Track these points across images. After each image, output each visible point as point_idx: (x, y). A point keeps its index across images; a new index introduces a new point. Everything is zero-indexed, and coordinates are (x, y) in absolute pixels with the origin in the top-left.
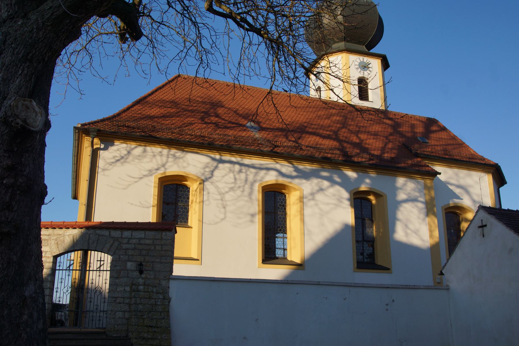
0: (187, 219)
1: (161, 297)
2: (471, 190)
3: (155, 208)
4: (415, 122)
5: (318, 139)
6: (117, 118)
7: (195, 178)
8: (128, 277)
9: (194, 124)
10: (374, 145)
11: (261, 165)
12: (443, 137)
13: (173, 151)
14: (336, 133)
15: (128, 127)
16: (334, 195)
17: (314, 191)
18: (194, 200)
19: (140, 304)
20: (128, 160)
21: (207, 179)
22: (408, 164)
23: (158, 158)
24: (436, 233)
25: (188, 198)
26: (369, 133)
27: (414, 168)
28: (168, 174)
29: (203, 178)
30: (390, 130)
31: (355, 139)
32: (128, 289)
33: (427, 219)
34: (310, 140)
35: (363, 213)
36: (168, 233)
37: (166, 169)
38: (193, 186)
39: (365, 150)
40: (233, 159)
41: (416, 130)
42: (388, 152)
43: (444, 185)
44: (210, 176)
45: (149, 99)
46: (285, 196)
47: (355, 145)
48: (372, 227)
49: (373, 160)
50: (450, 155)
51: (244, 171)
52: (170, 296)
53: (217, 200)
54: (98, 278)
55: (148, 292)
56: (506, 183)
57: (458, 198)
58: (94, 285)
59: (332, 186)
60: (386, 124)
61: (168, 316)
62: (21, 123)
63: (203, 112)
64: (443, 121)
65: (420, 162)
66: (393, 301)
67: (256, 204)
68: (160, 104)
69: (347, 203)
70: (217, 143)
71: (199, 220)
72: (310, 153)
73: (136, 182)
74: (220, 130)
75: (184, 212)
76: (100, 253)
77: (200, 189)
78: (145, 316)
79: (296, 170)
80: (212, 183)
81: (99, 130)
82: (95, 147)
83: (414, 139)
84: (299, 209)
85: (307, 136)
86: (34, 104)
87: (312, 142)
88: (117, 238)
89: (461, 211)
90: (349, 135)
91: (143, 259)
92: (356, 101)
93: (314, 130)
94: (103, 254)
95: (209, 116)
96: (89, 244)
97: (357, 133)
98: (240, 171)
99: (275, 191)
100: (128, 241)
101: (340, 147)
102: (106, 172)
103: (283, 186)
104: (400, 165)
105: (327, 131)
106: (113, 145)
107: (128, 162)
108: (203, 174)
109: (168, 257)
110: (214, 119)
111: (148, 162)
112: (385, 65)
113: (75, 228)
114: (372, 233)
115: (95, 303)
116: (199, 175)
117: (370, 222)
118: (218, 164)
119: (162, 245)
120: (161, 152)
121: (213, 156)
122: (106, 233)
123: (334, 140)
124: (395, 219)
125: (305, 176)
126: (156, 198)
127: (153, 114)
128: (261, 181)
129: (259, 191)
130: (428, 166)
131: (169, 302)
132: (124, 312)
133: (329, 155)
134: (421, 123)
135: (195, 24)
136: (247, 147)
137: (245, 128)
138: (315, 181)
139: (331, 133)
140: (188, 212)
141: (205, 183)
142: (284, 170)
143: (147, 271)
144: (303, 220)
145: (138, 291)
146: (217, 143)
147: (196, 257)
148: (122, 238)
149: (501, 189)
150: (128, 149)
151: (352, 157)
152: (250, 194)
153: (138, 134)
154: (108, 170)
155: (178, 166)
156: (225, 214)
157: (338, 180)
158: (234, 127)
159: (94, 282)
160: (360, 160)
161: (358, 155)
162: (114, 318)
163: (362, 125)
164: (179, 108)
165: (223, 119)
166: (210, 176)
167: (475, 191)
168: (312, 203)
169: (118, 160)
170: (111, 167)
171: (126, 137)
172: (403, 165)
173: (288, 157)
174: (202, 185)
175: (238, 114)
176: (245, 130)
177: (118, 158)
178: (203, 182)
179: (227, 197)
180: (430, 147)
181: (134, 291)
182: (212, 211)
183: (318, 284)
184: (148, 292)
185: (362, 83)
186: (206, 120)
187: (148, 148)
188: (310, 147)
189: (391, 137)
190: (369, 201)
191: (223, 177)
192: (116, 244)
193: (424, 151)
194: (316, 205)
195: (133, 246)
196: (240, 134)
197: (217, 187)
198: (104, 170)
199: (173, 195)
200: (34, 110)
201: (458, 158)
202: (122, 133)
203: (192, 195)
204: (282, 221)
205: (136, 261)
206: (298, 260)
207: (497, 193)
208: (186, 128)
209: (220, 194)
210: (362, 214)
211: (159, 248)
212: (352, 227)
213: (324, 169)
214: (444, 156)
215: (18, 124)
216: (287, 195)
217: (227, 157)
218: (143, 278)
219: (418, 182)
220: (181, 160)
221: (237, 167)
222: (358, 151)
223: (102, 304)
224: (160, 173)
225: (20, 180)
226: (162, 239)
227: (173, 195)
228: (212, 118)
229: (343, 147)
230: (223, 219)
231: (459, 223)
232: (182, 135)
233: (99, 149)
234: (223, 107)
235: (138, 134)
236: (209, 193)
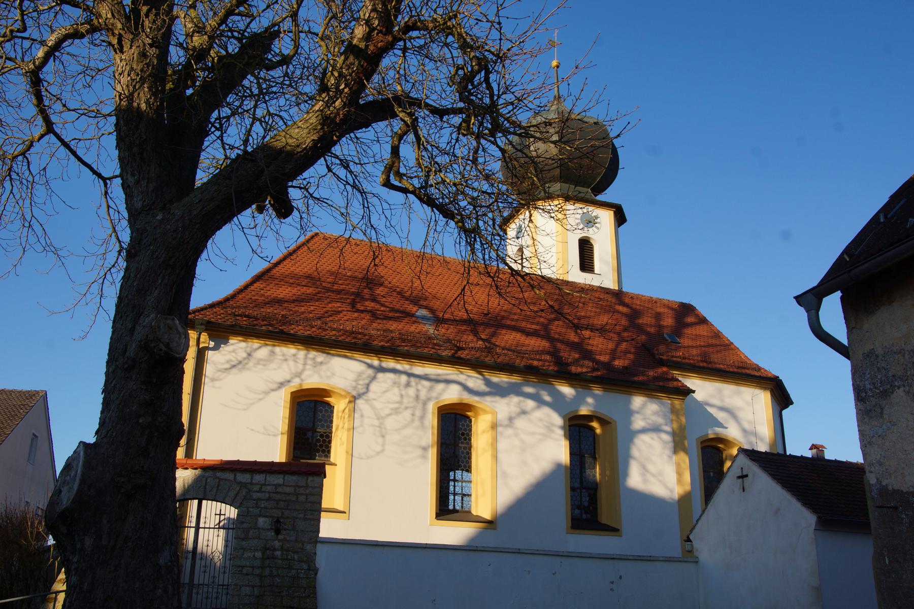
0: (329, 452)
1: (305, 566)
2: (740, 414)
3: (285, 437)
4: (662, 310)
5: (518, 336)
6: (231, 303)
7: (343, 393)
8: (259, 538)
9: (341, 312)
10: (599, 344)
11: (438, 375)
12: (702, 333)
13: (313, 354)
14: (546, 327)
15: (248, 316)
16: (541, 420)
17: (513, 415)
18: (341, 425)
19: (278, 575)
20: (247, 366)
21: (360, 396)
22: (648, 376)
23: (291, 363)
24: (687, 477)
25: (331, 422)
26: (592, 328)
27: (657, 383)
28: (305, 387)
29: (354, 393)
30: (624, 322)
31: (572, 337)
32: (259, 554)
33: (674, 457)
34: (508, 338)
35: (582, 447)
36: (316, 479)
37: (302, 380)
38: (339, 405)
39: (587, 355)
40: (399, 367)
41: (662, 323)
42: (619, 358)
43: (701, 407)
44: (364, 390)
45: (274, 271)
46: (470, 421)
47: (574, 346)
48: (594, 468)
49: (598, 370)
50: (710, 363)
51: (413, 384)
52: (317, 566)
53: (374, 426)
54: (216, 538)
55: (287, 559)
56: (792, 403)
57: (721, 425)
58: (210, 549)
59: (538, 407)
60: (619, 312)
61: (315, 593)
62: (164, 348)
63: (353, 293)
64: (703, 309)
65: (666, 373)
66: (621, 577)
67: (427, 434)
68: (291, 281)
69: (561, 432)
70: (375, 343)
71: (347, 452)
72: (507, 358)
73: (261, 399)
74: (379, 321)
75: (324, 441)
76: (219, 504)
77: (349, 410)
78: (284, 594)
79: (488, 383)
80: (366, 400)
81: (209, 322)
82: (201, 346)
83: (658, 337)
84: (490, 441)
85: (504, 332)
86: (177, 322)
87: (510, 342)
88: (245, 484)
89: (725, 445)
90: (564, 330)
91: (280, 513)
92: (578, 277)
93: (513, 323)
94: (223, 505)
95: (364, 299)
96: (205, 491)
97: (577, 327)
98: (408, 385)
99: (456, 414)
100: (261, 488)
101: (551, 350)
102: (217, 384)
103: (469, 407)
104: (636, 379)
105: (533, 323)
106: (226, 343)
107: (248, 369)
108: (355, 388)
109: (313, 508)
110: (370, 305)
111: (275, 369)
112: (620, 218)
113: (187, 469)
114: (595, 476)
115: (212, 574)
116: (350, 389)
117: (591, 459)
118: (376, 373)
119: (306, 495)
120: (294, 355)
121: (369, 361)
122: (230, 476)
123: (542, 337)
124: (628, 457)
125: (501, 392)
126: (287, 421)
127: (281, 296)
128: (437, 398)
129: (433, 413)
130: (677, 380)
131: (316, 574)
132: (253, 586)
133: (535, 363)
134: (670, 312)
135: (362, 193)
136: (419, 350)
137: (414, 319)
138: (515, 399)
139: (538, 327)
140: (330, 442)
141: (358, 401)
142: (471, 384)
143: (285, 530)
144: (495, 457)
145: (274, 558)
146: (375, 343)
147: (341, 509)
148: (251, 483)
149: (784, 412)
150: (249, 350)
151: (568, 365)
152: (422, 418)
153: (264, 328)
154: (220, 380)
155: (320, 376)
156: (383, 445)
157: (547, 398)
158: (398, 317)
159: (210, 544)
160: (579, 370)
161: (576, 362)
162: (239, 595)
163: (583, 314)
164: (319, 286)
165: (383, 305)
166: (364, 390)
167: (745, 415)
168: (510, 431)
169: (234, 366)
170: (225, 374)
171: (248, 333)
172: (641, 378)
173: (477, 365)
174: (352, 405)
175: (403, 297)
176: (415, 322)
177: (233, 363)
178: (354, 399)
179: (390, 423)
180: (682, 349)
181: (268, 558)
182: (365, 440)
183: (519, 552)
184: (287, 559)
185: (585, 247)
186: (359, 306)
187: (278, 349)
188: (508, 350)
189: (625, 334)
190: (592, 429)
191: (385, 392)
192: (244, 492)
193: (673, 357)
194: (516, 435)
195: (267, 495)
196: (407, 328)
197: (374, 408)
198: (213, 380)
199: (311, 419)
200: (177, 329)
201: (722, 366)
202: (241, 327)
203: (338, 418)
204: (465, 458)
205: (271, 517)
206: (487, 516)
207: (778, 415)
208: (331, 318)
209: (378, 419)
210: (580, 448)
211: (302, 498)
212: (566, 467)
213: (527, 383)
214: (701, 365)
215: (161, 350)
216: (473, 420)
217: (390, 363)
218: (280, 541)
219: (663, 404)
220: (324, 367)
221: (404, 378)
222: (577, 356)
223: (221, 576)
224: (295, 385)
225: (159, 419)
226: (307, 486)
227: (311, 419)
228: (367, 303)
229: (555, 347)
230: (379, 453)
231: (722, 464)
232: (325, 330)
233: (207, 348)
234: (381, 285)
235: (264, 328)
236: (362, 416)
